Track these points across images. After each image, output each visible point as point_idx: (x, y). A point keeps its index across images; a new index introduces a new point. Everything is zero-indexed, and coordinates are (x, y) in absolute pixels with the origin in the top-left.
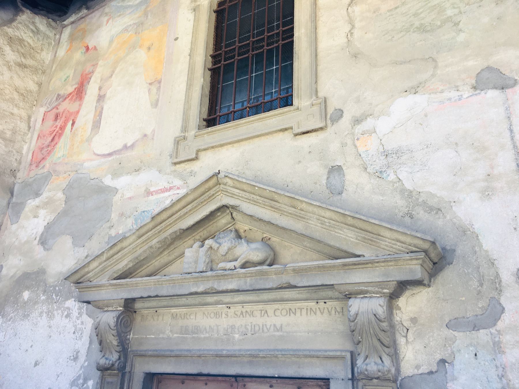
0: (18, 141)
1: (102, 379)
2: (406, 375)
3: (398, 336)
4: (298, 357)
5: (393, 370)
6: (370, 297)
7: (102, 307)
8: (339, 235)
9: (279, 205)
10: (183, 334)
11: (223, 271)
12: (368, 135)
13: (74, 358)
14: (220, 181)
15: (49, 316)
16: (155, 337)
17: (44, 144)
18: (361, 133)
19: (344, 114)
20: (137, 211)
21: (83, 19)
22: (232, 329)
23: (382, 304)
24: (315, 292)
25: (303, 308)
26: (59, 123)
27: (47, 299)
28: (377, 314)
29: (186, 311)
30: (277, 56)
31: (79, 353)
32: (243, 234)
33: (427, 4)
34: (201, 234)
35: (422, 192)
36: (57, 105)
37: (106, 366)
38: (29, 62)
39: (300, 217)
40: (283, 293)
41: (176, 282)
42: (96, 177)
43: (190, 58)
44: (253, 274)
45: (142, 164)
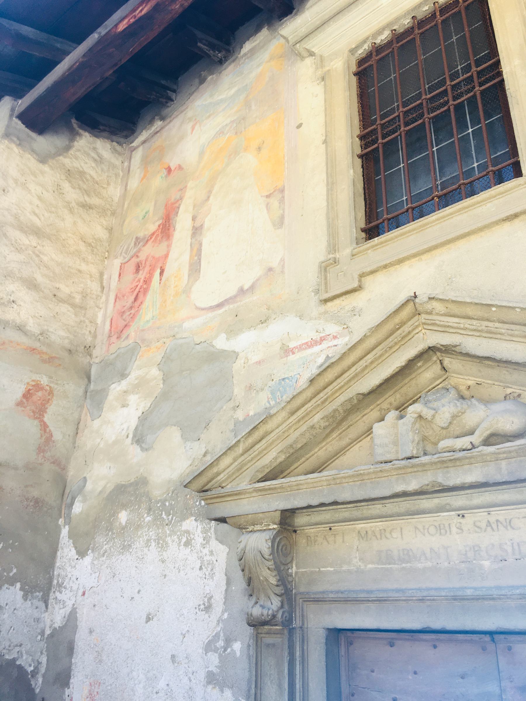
0: (90, 308)
1: (257, 638)
7: (244, 526)
10: (383, 564)
11: (452, 453)
13: (206, 608)
15: (160, 545)
16: (334, 570)
17: (124, 306)
20: (273, 380)
21: (158, 134)
26: (142, 275)
27: (155, 520)
29: (382, 525)
31: (212, 599)
34: (392, 399)
37: (263, 618)
38: (95, 201)
44: (512, 454)
45: (271, 311)
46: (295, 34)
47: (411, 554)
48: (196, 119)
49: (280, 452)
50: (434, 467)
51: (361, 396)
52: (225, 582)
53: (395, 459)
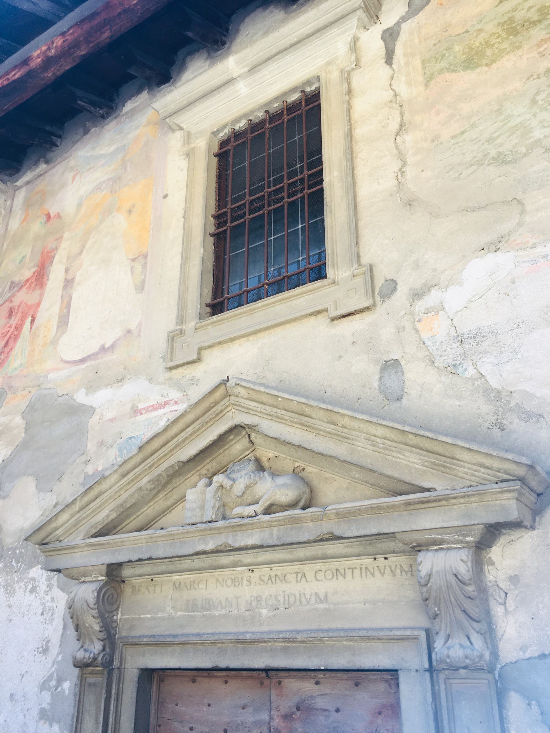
1: (82, 678)
2: (508, 661)
3: (493, 604)
4: (351, 640)
5: (487, 656)
6: (448, 549)
7: (76, 577)
8: (398, 460)
9: (312, 421)
11: (238, 520)
12: (433, 313)
13: (43, 650)
14: (230, 391)
15: (8, 591)
16: (151, 617)
18: (423, 312)
19: (398, 287)
20: (121, 438)
21: (42, 178)
22: (257, 601)
23: (465, 558)
24: (371, 544)
25: (356, 568)
27: (5, 566)
28: (457, 573)
29: (193, 577)
30: (303, 210)
31: (50, 643)
32: (266, 464)
33: (505, 124)
34: (209, 466)
35: (514, 392)
36: (10, 297)
39: (342, 437)
40: (325, 546)
41: (176, 537)
42: (65, 393)
43: (185, 221)
46: (165, 109)
47: (211, 603)
48: (77, 169)
49: (111, 510)
50: (227, 531)
51: (182, 464)
52: (62, 627)
53: (200, 521)
